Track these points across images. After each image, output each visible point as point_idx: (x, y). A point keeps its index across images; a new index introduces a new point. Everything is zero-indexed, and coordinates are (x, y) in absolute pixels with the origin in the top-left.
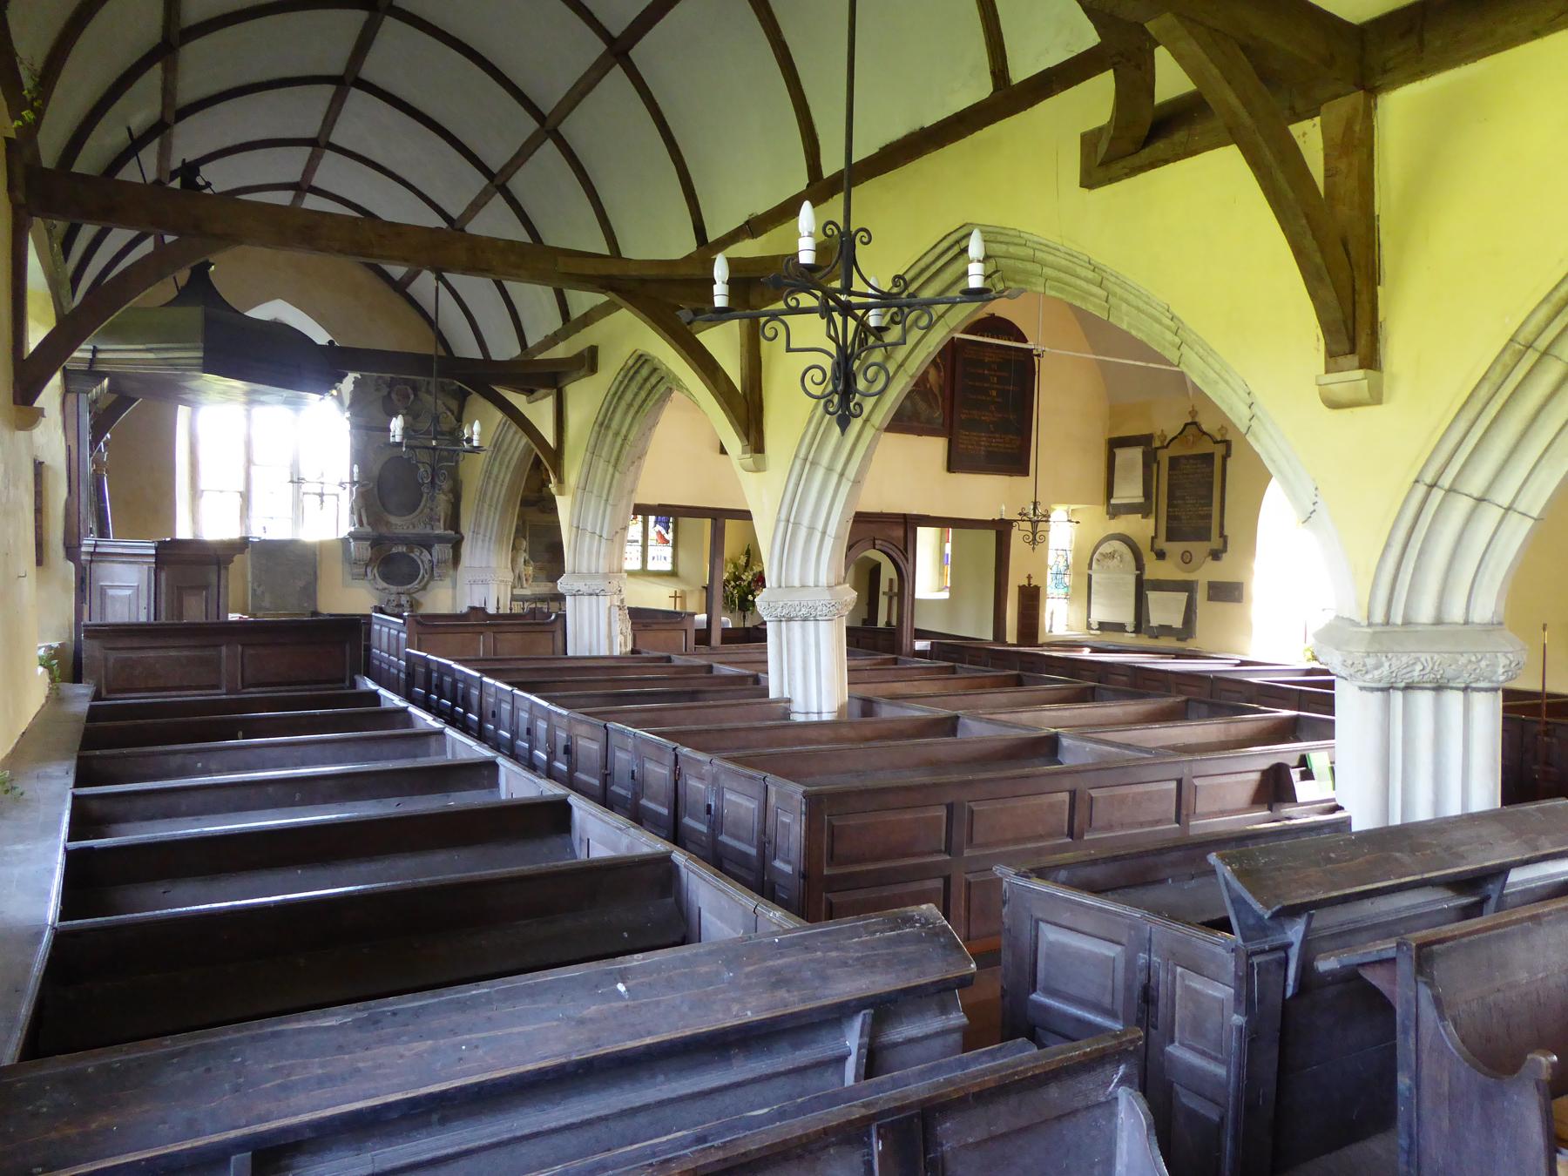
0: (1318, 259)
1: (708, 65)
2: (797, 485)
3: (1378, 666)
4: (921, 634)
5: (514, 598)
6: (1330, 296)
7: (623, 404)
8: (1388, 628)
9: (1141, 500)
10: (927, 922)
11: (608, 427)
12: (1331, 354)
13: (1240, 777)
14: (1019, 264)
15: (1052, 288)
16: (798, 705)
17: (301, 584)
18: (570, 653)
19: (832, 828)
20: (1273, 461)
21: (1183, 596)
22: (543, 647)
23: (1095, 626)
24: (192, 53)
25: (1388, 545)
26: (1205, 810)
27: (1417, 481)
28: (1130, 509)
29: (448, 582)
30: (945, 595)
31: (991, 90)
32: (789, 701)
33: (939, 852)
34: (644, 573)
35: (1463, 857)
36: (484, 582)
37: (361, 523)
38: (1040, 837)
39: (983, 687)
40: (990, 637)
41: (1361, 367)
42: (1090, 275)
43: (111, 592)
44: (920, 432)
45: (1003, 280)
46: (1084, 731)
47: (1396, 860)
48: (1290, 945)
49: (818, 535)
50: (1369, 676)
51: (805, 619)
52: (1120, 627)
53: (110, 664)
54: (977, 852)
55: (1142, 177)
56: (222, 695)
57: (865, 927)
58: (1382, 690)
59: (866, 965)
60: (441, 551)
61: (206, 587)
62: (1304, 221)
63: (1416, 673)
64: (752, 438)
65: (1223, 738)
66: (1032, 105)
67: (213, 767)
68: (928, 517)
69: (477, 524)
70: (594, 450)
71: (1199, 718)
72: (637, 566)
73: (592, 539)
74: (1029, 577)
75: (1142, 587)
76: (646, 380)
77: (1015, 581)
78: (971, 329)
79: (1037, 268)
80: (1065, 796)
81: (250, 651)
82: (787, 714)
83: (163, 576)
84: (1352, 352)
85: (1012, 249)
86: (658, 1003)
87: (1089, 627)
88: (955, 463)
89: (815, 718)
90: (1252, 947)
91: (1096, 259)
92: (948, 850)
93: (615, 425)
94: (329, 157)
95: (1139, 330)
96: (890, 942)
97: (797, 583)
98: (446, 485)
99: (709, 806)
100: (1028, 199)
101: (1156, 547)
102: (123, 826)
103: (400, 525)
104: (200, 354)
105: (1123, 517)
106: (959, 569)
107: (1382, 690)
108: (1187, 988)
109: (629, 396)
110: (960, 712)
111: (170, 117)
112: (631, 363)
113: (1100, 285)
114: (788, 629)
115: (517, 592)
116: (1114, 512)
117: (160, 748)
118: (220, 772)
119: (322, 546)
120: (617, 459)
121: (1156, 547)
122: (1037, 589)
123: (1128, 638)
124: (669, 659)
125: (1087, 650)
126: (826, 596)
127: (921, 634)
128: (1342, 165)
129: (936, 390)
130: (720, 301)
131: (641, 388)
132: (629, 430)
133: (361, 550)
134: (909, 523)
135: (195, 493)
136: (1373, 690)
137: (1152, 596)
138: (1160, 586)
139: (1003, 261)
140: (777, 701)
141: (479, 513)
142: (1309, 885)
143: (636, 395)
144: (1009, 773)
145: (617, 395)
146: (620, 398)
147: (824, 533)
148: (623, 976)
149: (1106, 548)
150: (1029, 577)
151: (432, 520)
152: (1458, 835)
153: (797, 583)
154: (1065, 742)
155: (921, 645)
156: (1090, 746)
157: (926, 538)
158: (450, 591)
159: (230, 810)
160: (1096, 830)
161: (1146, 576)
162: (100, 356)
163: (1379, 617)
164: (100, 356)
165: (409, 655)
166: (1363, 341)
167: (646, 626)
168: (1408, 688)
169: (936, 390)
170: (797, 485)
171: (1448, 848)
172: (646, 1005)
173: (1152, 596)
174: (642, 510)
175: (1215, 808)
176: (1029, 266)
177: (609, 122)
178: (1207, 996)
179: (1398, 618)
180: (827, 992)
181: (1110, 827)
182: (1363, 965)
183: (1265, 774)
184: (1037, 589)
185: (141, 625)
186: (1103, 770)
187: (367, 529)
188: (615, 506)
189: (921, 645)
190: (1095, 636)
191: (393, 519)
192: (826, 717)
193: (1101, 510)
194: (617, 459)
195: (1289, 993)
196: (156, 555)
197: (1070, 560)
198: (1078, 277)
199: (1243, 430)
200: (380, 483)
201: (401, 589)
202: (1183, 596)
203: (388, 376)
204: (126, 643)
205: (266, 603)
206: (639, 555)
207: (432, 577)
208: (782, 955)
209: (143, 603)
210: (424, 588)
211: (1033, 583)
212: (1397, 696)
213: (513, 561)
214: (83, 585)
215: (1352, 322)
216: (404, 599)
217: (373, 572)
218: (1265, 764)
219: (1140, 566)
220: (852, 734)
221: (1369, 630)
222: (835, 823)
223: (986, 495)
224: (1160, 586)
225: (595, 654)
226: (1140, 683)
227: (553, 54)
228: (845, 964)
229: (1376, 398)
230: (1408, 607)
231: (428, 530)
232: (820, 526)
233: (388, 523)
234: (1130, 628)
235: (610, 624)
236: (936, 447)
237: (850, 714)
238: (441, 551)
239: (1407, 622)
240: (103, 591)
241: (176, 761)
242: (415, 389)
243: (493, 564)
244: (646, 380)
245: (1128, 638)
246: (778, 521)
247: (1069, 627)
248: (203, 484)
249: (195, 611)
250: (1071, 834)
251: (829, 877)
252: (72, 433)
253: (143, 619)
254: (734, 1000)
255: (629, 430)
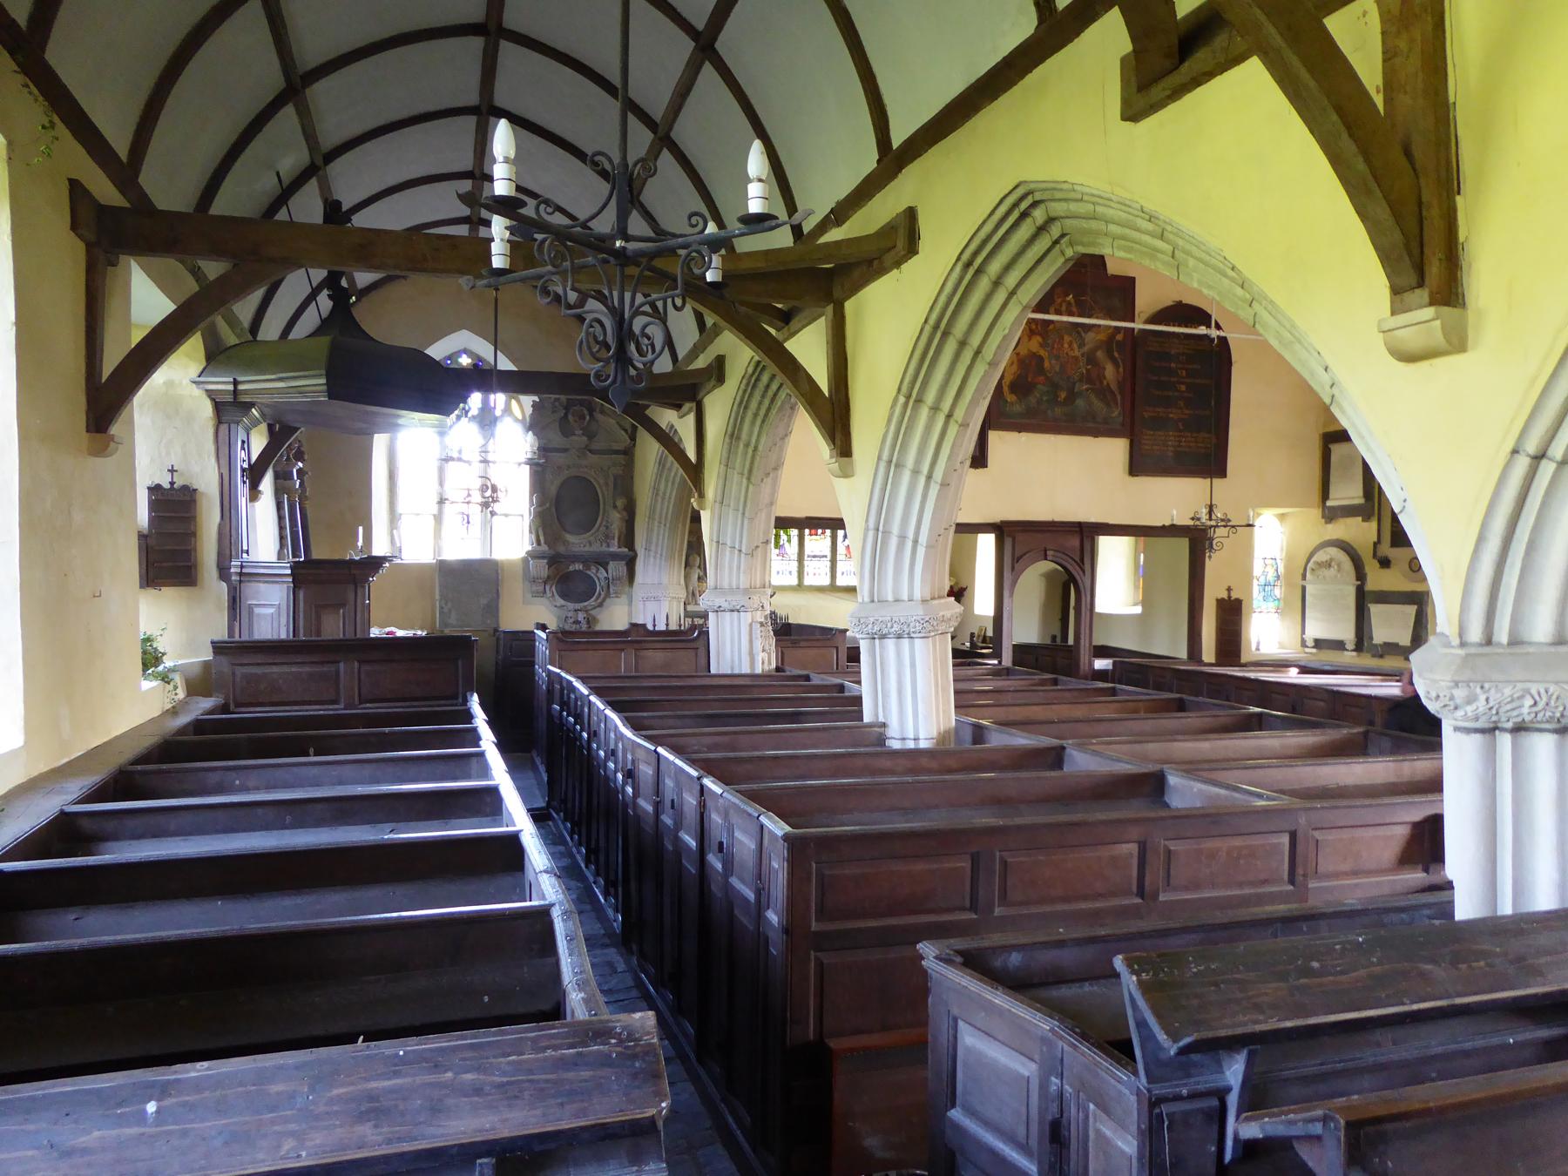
0: (1361, 165)
1: (783, 45)
2: (884, 490)
3: (1470, 700)
4: (1102, 651)
5: (687, 614)
6: (1382, 212)
7: (750, 414)
8: (1487, 650)
9: (1362, 501)
10: (630, 1037)
11: (738, 438)
12: (1396, 291)
13: (1381, 831)
14: (1084, 224)
15: (1119, 248)
16: (893, 731)
17: (484, 601)
18: (713, 671)
19: (821, 877)
20: (1362, 438)
21: (1411, 610)
22: (683, 661)
23: (1310, 643)
24: (321, 93)
25: (1481, 539)
26: (1331, 868)
27: (1515, 452)
28: (1349, 511)
29: (624, 598)
30: (1138, 610)
31: (1035, 23)
32: (884, 725)
33: (963, 909)
34: (833, 588)
35: (1541, 974)
36: (656, 599)
37: (539, 543)
38: (1099, 896)
39: (1136, 711)
40: (1183, 654)
41: (1431, 304)
42: (1150, 227)
43: (257, 610)
44: (1096, 433)
45: (1071, 244)
46: (1192, 768)
47: (1422, 974)
48: (1229, 1090)
49: (909, 544)
50: (1460, 713)
51: (899, 637)
52: (1339, 645)
53: (238, 679)
54: (1013, 911)
55: (1189, 99)
56: (339, 709)
57: (534, 1040)
58: (1482, 731)
59: (509, 1093)
60: (617, 569)
61: (343, 605)
62: (1335, 117)
63: (1525, 710)
64: (838, 442)
65: (1393, 779)
66: (1078, 35)
67: (250, 784)
68: (1107, 525)
69: (649, 541)
70: (728, 463)
71: (1382, 753)
72: (826, 581)
73: (732, 553)
74: (1229, 589)
75: (1363, 600)
76: (768, 387)
77: (1213, 592)
78: (1041, 307)
79: (1102, 226)
80: (1133, 848)
81: (366, 668)
82: (881, 740)
83: (301, 595)
84: (1421, 285)
85: (1073, 207)
86: (185, 1133)
87: (1304, 644)
88: (1137, 466)
89: (911, 745)
90: (1160, 1090)
91: (1149, 206)
92: (973, 908)
93: (744, 436)
94: (337, 168)
95: (1210, 287)
96: (563, 1064)
97: (890, 598)
98: (620, 503)
99: (721, 844)
100: (1080, 140)
101: (1379, 554)
102: (109, 844)
103: (577, 543)
104: (323, 381)
105: (1342, 521)
106: (1148, 580)
107: (1482, 731)
108: (1098, 1131)
109: (754, 405)
110: (1064, 743)
111: (319, 161)
112: (750, 370)
113: (1162, 237)
114: (882, 647)
115: (690, 608)
116: (1331, 515)
117: (198, 764)
118: (257, 789)
119: (511, 563)
120: (750, 471)
121: (1379, 554)
122: (1239, 602)
123: (1349, 657)
124: (807, 678)
125: (1294, 671)
126: (919, 611)
127: (1102, 651)
128: (1403, 44)
129: (1114, 387)
130: (498, 262)
131: (763, 396)
132: (758, 441)
133: (541, 568)
134: (1085, 535)
135: (394, 518)
136: (1476, 731)
137: (1375, 610)
138: (1385, 597)
139: (1068, 222)
140: (870, 726)
141: (650, 530)
142: (1258, 1008)
143: (760, 403)
144: (1114, 815)
145: (742, 405)
146: (746, 408)
147: (916, 542)
148: (162, 1091)
149: (1321, 556)
150: (1229, 589)
151: (608, 537)
152: (1544, 940)
153: (890, 598)
154: (1173, 780)
155: (1101, 664)
156: (1198, 786)
157: (1105, 543)
158: (626, 608)
159: (217, 832)
160: (1175, 889)
161: (1370, 586)
162: (241, 387)
163: (1475, 634)
164: (241, 387)
165: (549, 673)
166: (1434, 269)
167: (795, 644)
168: (1519, 729)
169: (1114, 387)
170: (884, 490)
171: (1519, 959)
172: (170, 1133)
173: (1375, 610)
174: (783, 523)
175: (1346, 867)
176: (1094, 225)
177: (708, 114)
178: (1117, 1147)
179: (1502, 636)
180: (431, 1130)
181: (1196, 885)
182: (1298, 1138)
183: (1417, 827)
184: (1239, 602)
185: (282, 641)
186: (1210, 821)
187: (544, 548)
188: (751, 519)
189: (1101, 664)
190: (1310, 655)
191: (571, 538)
192: (923, 745)
193: (1316, 513)
194: (750, 471)
195: (1228, 1157)
196: (292, 574)
197: (1281, 570)
198: (1138, 230)
199: (1327, 401)
200: (558, 501)
201: (578, 606)
202: (1411, 610)
203: (563, 398)
204: (259, 658)
205: (453, 620)
206: (828, 570)
207: (608, 595)
208: (396, 1074)
209: (283, 620)
210: (601, 605)
211: (1234, 596)
212: (1505, 741)
213: (686, 577)
214: (235, 602)
215: (1422, 246)
216: (581, 616)
217: (551, 589)
218: (1417, 815)
219: (1360, 575)
220: (934, 765)
221: (1461, 652)
222: (827, 872)
223: (1175, 499)
224: (1385, 597)
225: (736, 671)
226: (1340, 705)
227: (659, 56)
228: (478, 1091)
229: (1457, 343)
230: (1516, 619)
231: (604, 548)
232: (911, 535)
233: (566, 543)
234: (1351, 646)
235: (751, 641)
236: (1115, 450)
237: (958, 739)
238: (617, 569)
239: (1515, 641)
240: (251, 607)
241: (213, 778)
242: (591, 411)
243: (665, 580)
244: (768, 387)
245: (1349, 657)
246: (867, 529)
247: (1282, 646)
248: (401, 507)
249: (334, 628)
250: (1141, 892)
251: (816, 934)
252: (224, 461)
253: (283, 636)
254: (292, 1134)
255: (758, 441)
